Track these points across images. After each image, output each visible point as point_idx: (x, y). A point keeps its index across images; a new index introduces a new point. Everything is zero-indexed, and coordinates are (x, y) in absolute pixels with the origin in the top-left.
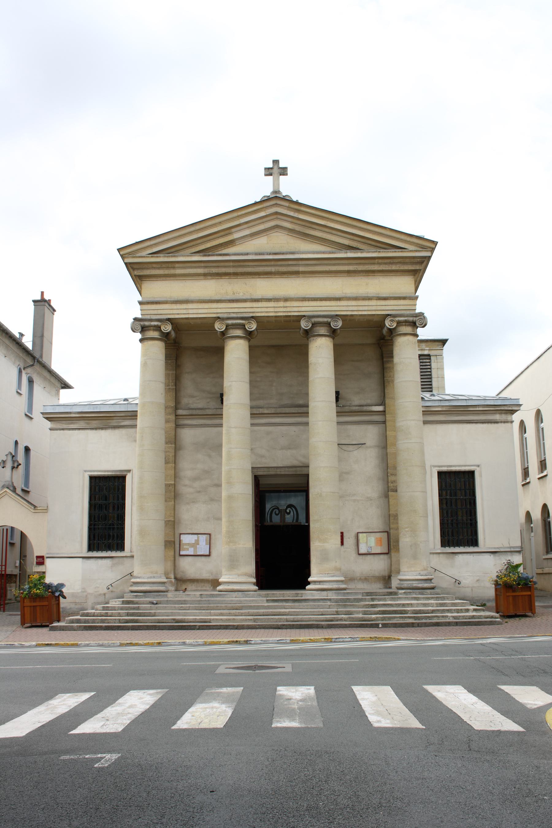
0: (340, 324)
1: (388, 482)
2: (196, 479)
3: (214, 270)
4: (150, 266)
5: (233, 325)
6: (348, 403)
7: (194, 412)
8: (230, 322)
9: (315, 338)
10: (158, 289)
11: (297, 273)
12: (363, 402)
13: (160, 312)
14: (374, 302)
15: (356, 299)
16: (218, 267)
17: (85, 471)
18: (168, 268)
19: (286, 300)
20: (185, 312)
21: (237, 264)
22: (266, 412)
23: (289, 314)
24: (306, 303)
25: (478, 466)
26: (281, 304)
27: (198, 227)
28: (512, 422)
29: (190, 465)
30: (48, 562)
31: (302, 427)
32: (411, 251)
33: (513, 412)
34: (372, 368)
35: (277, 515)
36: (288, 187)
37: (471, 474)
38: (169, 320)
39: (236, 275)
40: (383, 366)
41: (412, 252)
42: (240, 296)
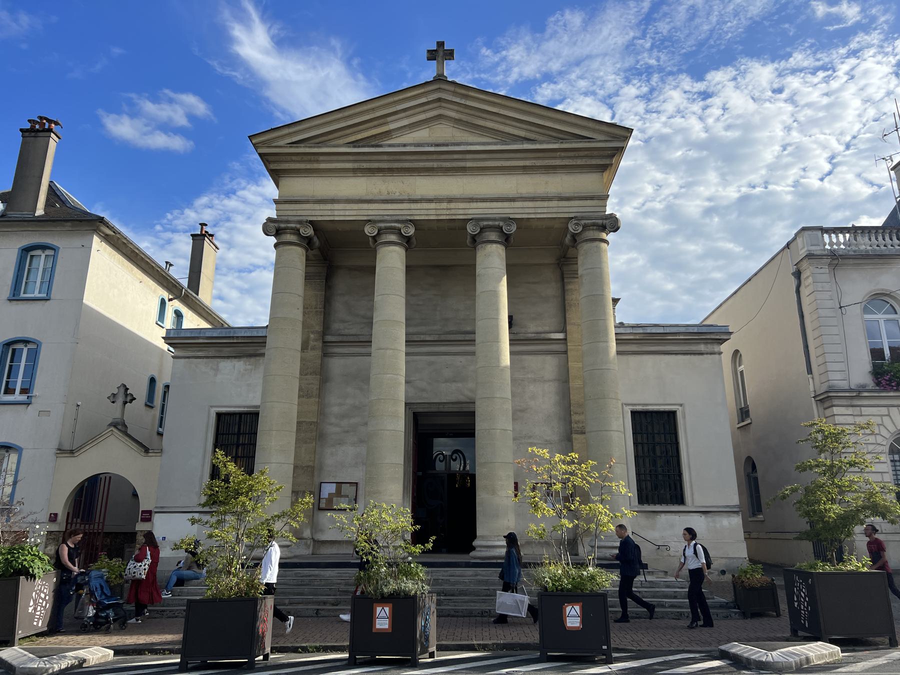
0: (514, 228)
1: (571, 422)
2: (343, 416)
3: (365, 165)
4: (289, 158)
5: (386, 228)
6: (523, 330)
7: (345, 339)
8: (383, 225)
9: (483, 245)
10: (300, 186)
11: (463, 170)
12: (540, 329)
13: (299, 213)
14: (554, 203)
15: (533, 199)
16: (370, 161)
17: (212, 407)
18: (310, 161)
19: (450, 200)
20: (329, 213)
21: (391, 158)
22: (428, 339)
23: (454, 217)
24: (474, 205)
25: (681, 405)
26: (444, 205)
27: (347, 113)
28: (720, 353)
29: (336, 403)
30: (157, 518)
31: (469, 357)
32: (600, 141)
33: (721, 341)
34: (550, 290)
35: (441, 461)
36: (452, 70)
37: (673, 414)
38: (311, 222)
39: (391, 171)
40: (564, 300)
41: (601, 142)
42: (397, 196)
